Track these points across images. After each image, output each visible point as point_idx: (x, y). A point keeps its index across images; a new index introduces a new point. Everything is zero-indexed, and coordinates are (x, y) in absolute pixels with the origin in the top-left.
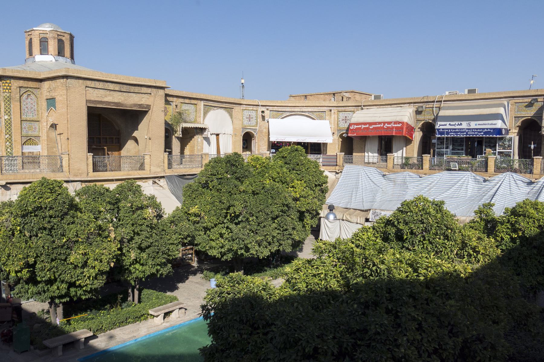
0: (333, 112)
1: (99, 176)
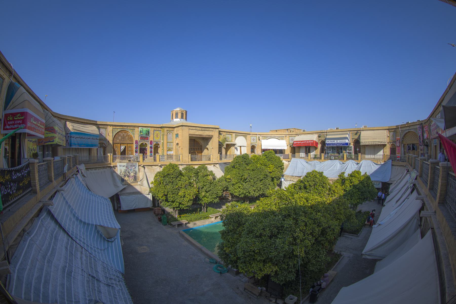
1: (193, 163)
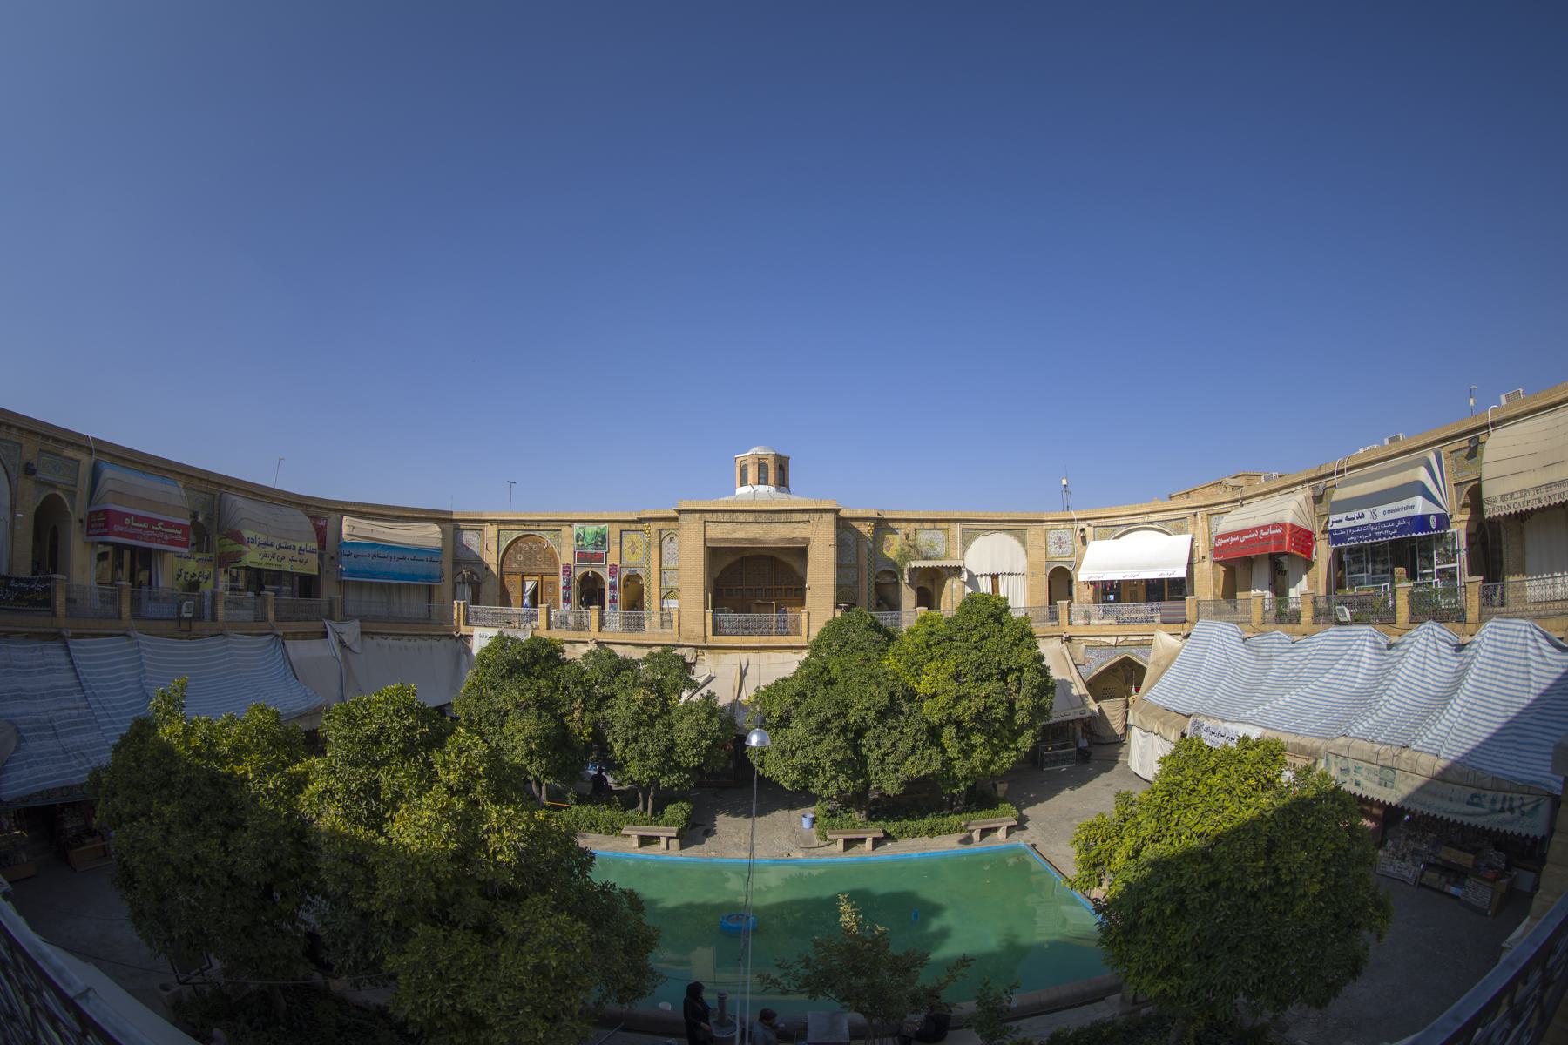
0: (1199, 516)
1: (722, 642)
